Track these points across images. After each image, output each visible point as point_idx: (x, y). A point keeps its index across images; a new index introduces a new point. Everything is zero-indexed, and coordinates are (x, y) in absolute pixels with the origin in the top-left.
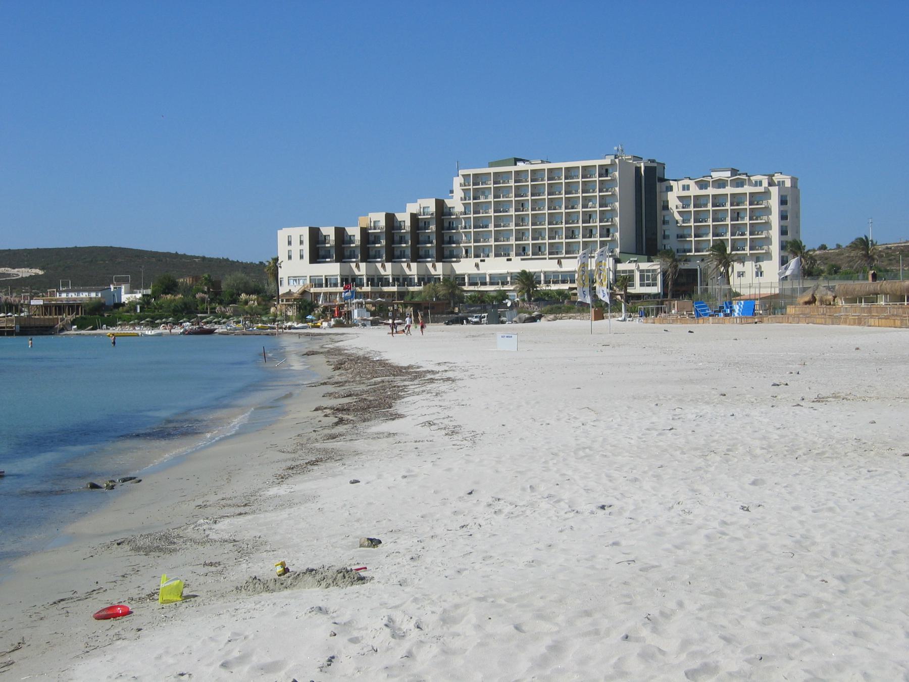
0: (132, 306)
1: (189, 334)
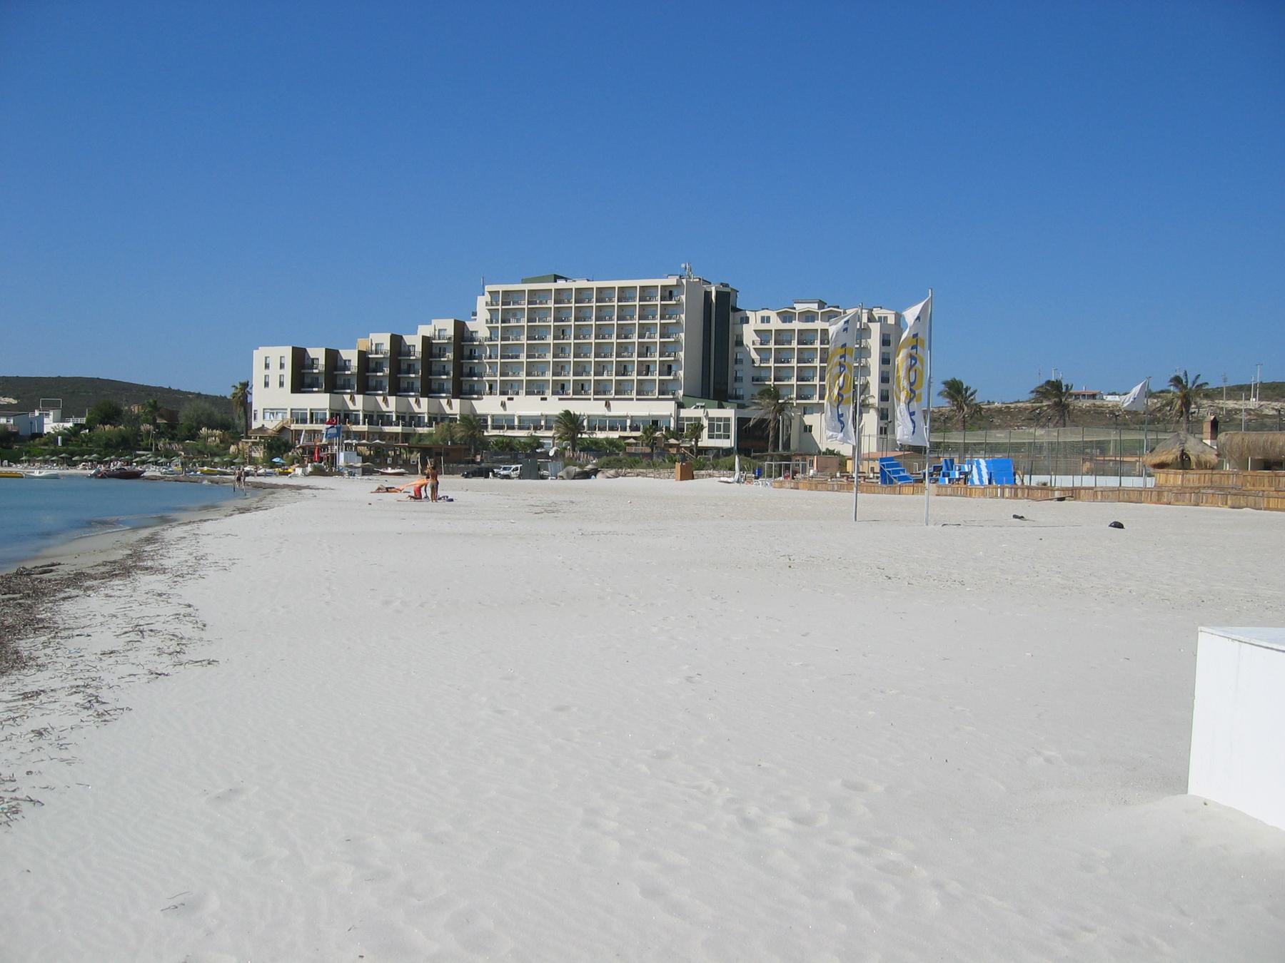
0: (52, 438)
1: (102, 477)
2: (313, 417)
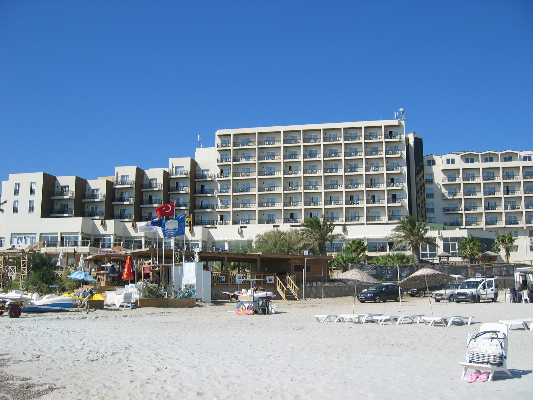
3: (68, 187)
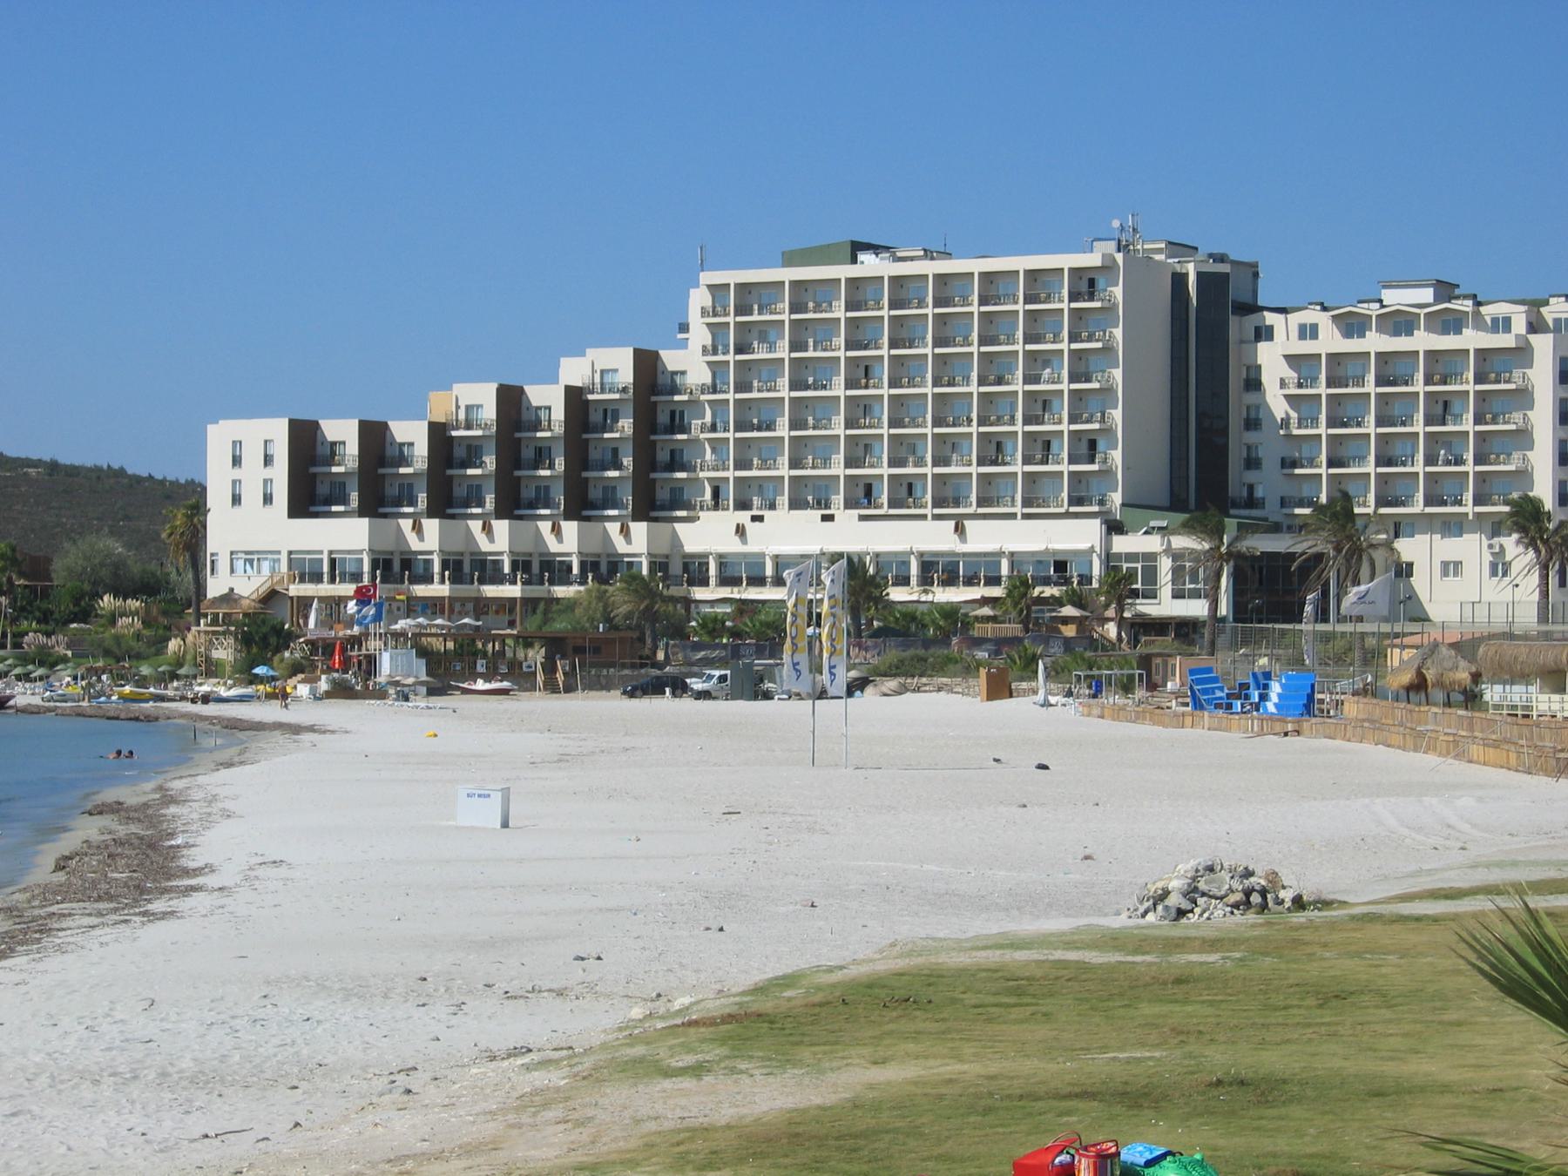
2: (337, 568)
3: (344, 443)
